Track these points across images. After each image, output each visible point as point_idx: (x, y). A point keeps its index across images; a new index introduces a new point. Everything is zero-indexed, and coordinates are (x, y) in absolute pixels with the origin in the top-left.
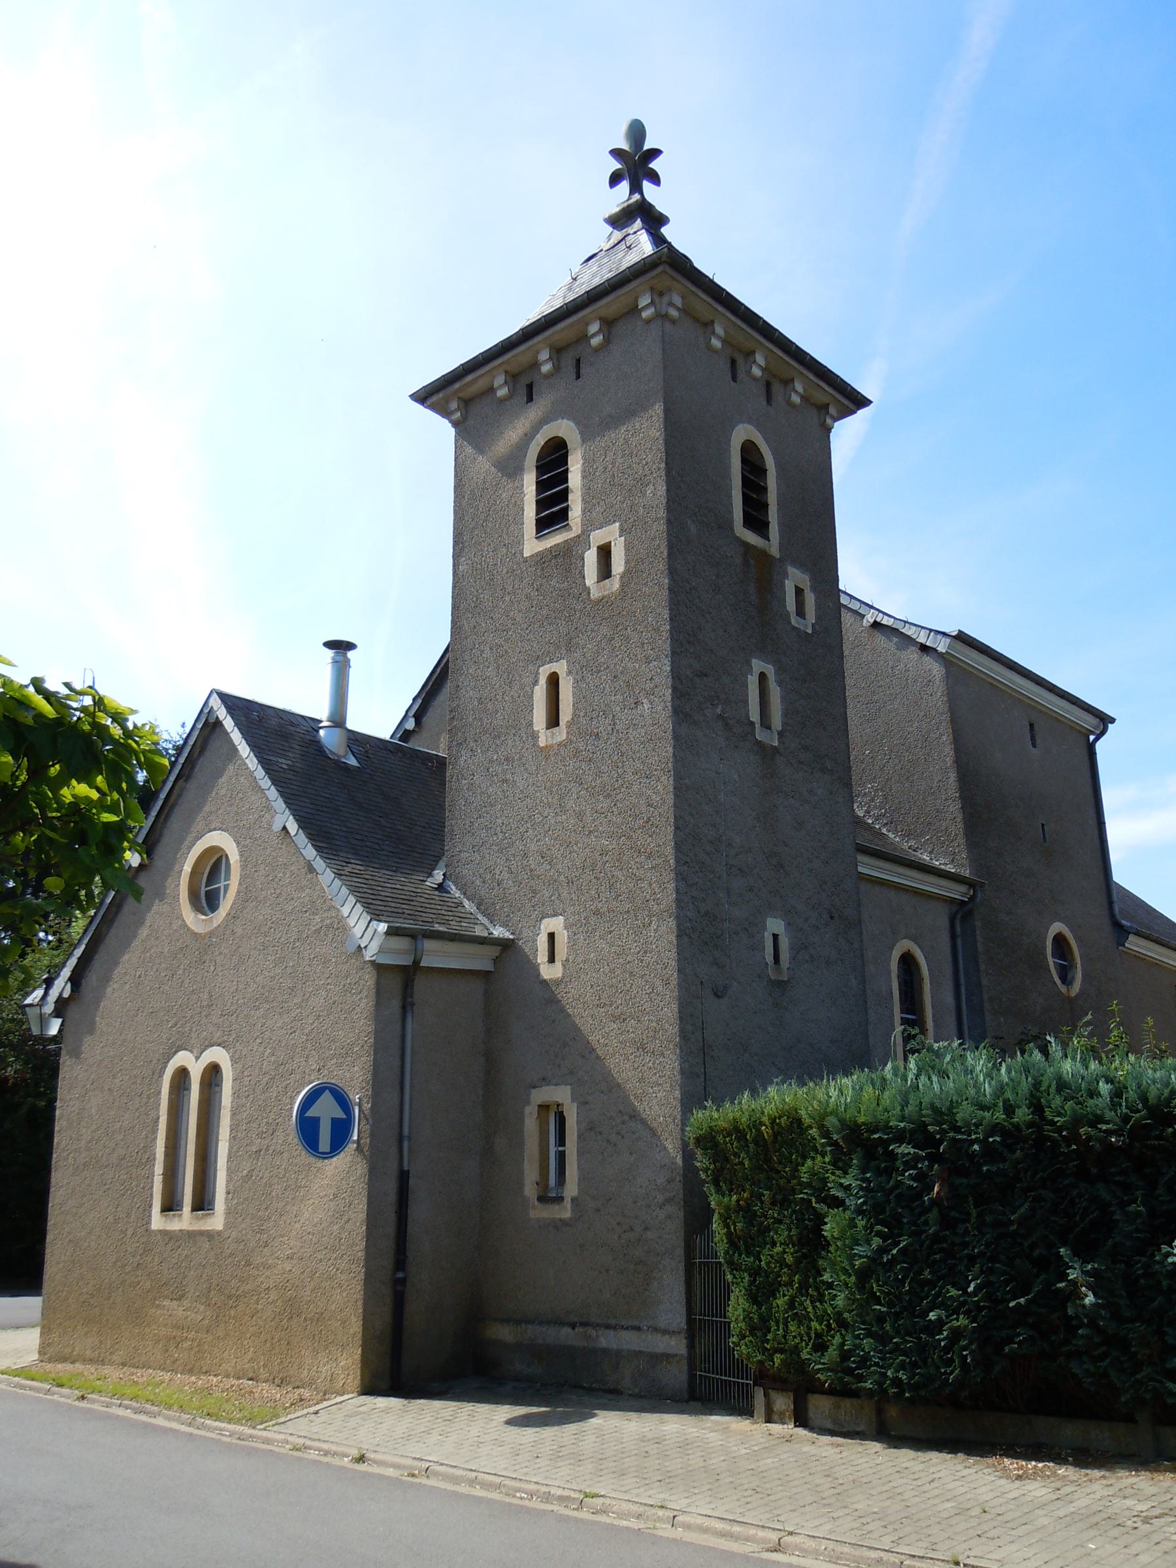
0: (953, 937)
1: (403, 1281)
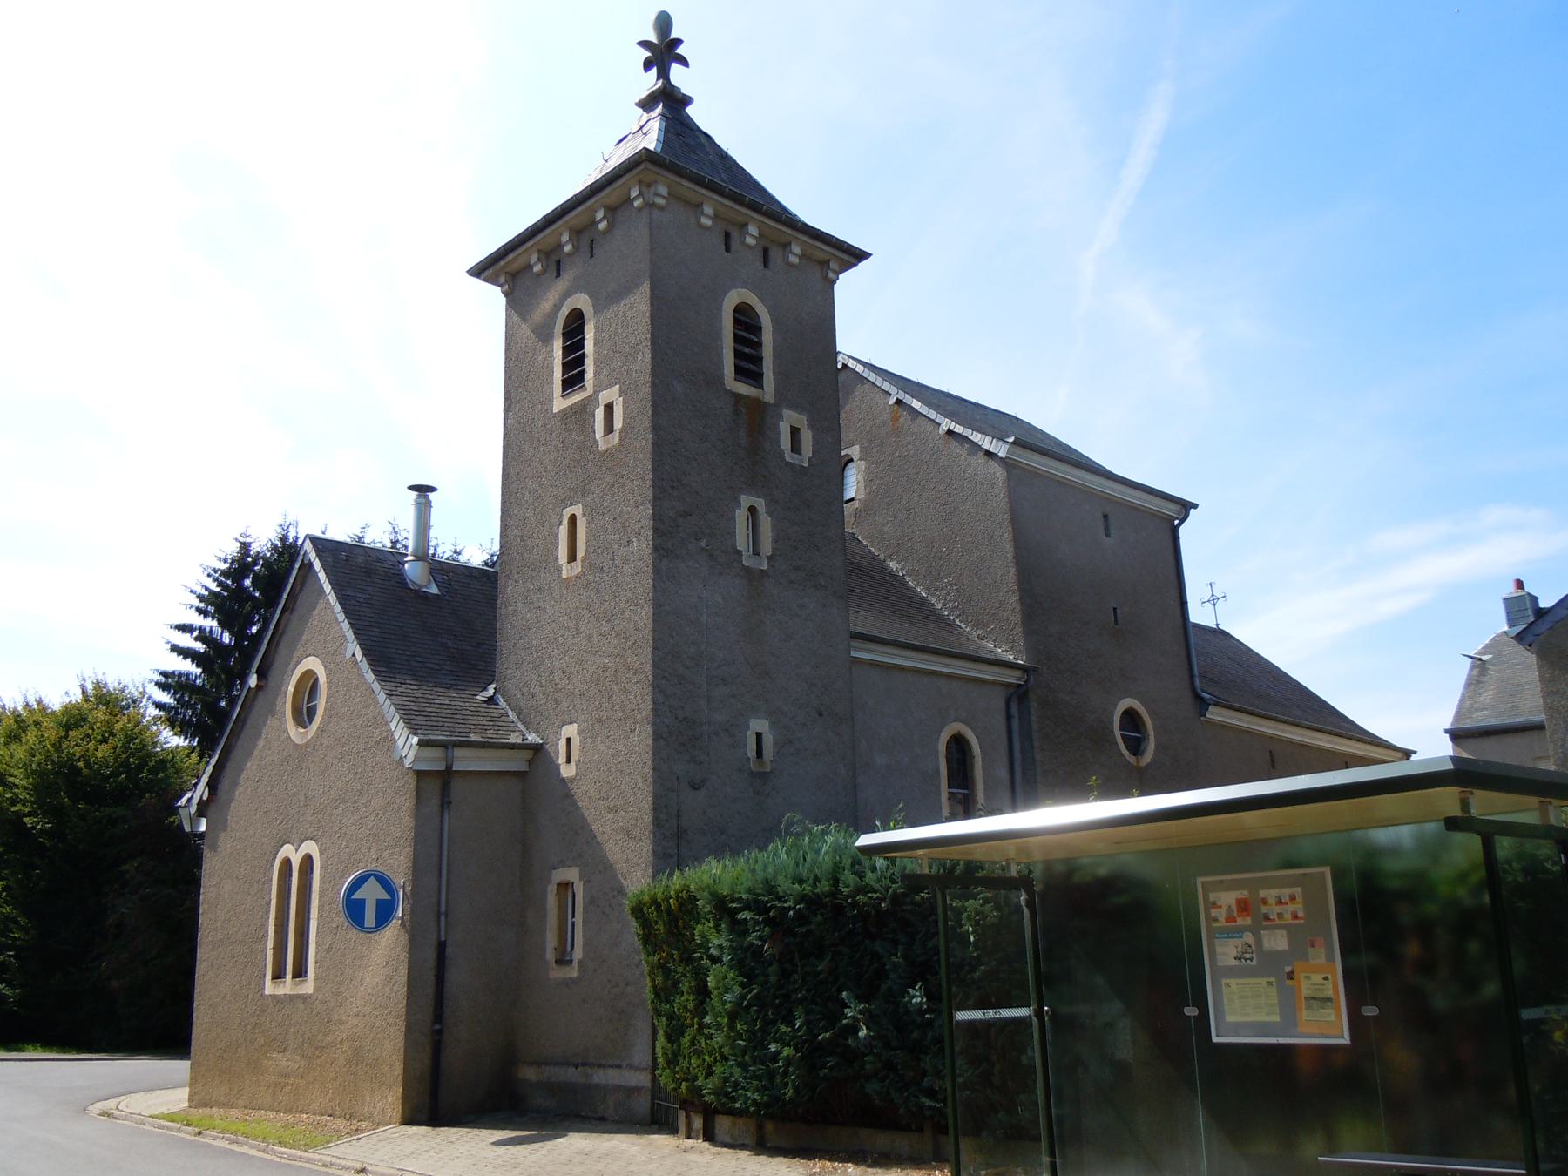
0: (1009, 717)
1: (440, 1032)
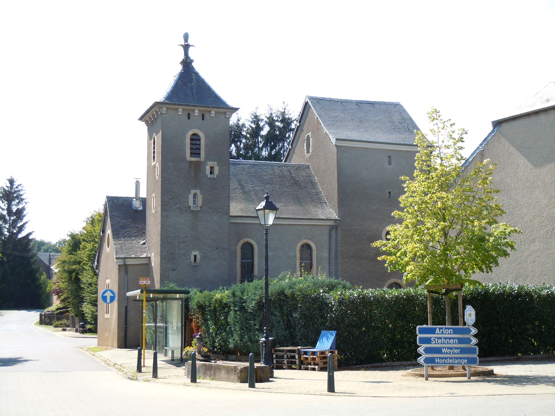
0: (330, 236)
1: (126, 327)
